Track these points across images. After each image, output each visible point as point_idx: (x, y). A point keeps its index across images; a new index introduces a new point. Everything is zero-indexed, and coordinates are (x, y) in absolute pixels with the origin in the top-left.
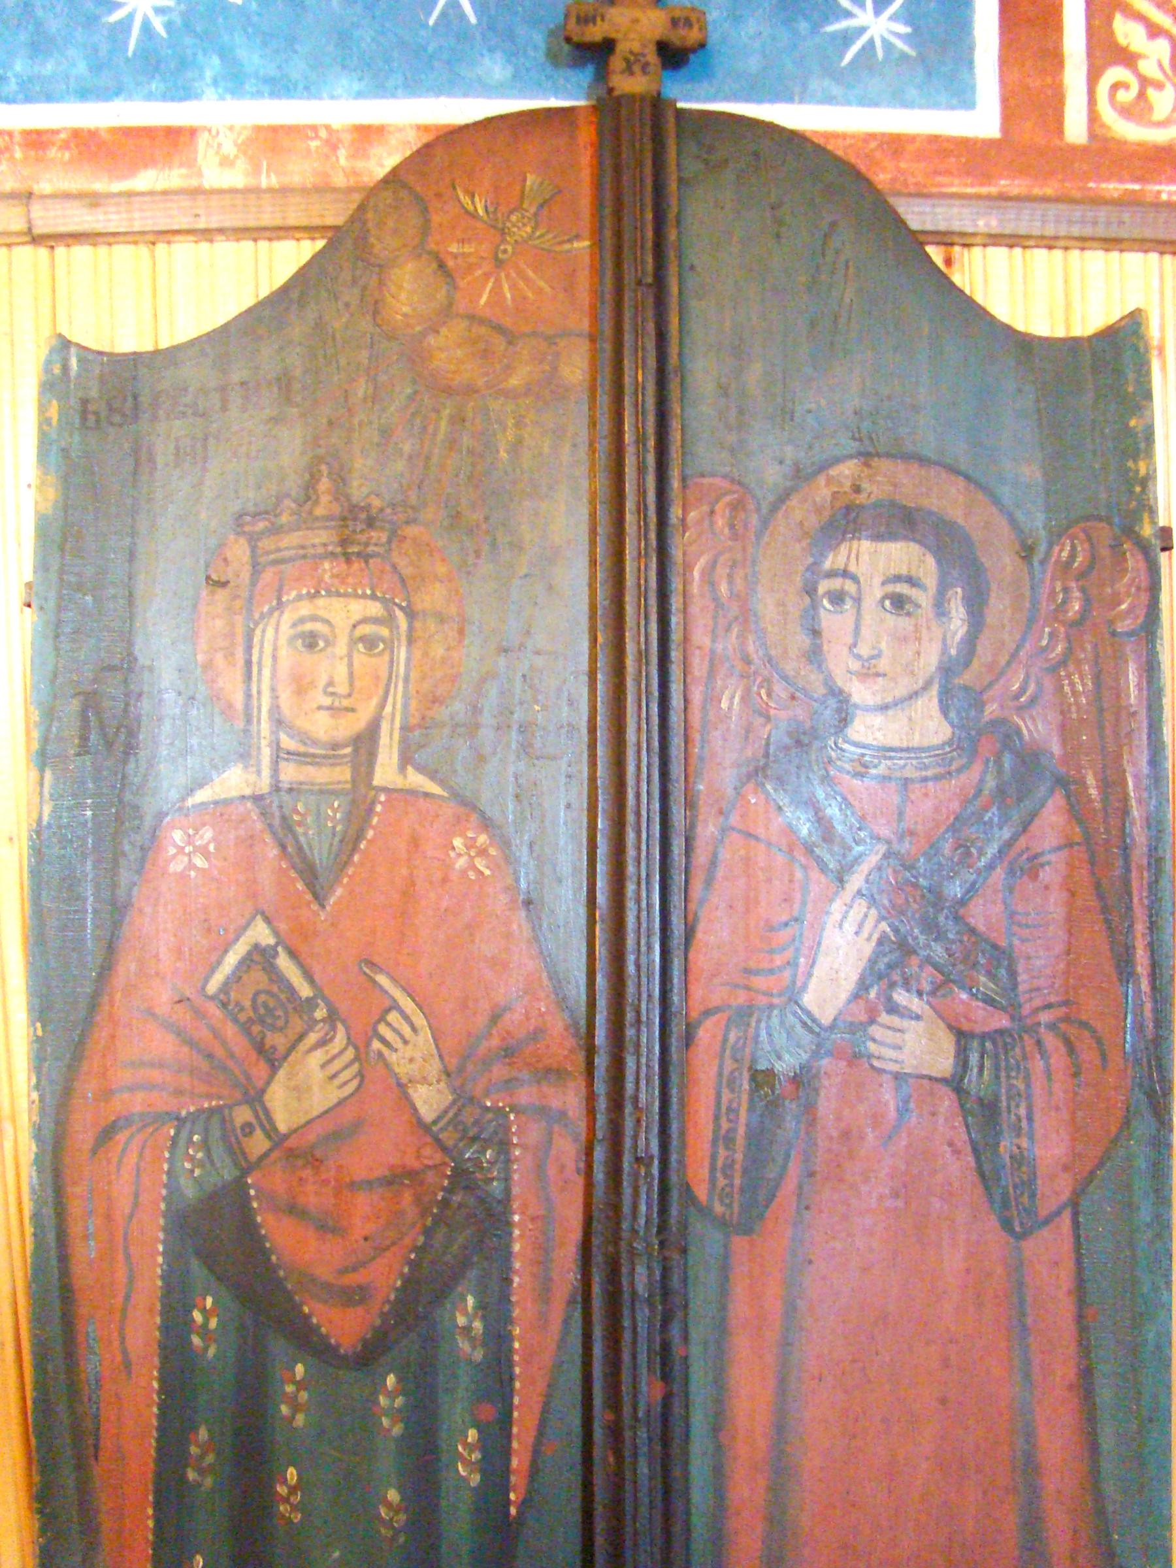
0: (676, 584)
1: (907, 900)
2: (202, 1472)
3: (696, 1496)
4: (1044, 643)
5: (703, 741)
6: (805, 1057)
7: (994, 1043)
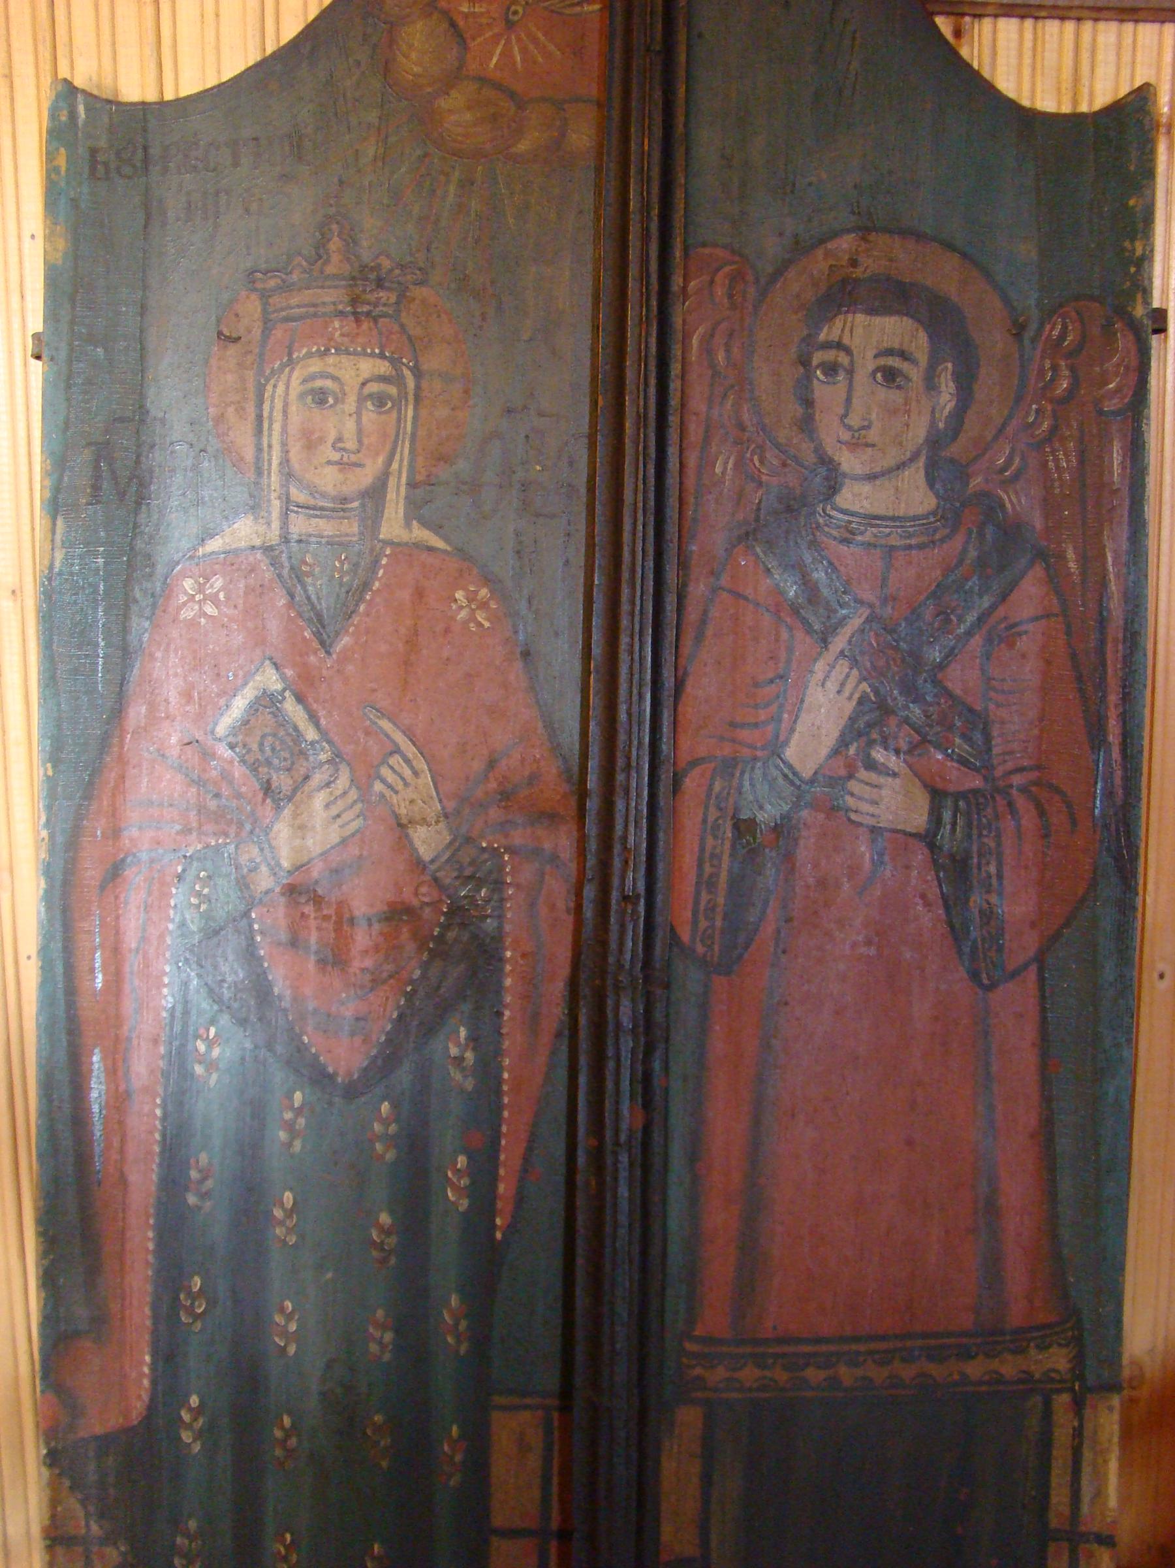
0: (676, 351)
1: (887, 662)
2: (205, 1196)
3: (673, 1225)
4: (1031, 419)
5: (697, 505)
6: (786, 808)
7: (968, 804)
